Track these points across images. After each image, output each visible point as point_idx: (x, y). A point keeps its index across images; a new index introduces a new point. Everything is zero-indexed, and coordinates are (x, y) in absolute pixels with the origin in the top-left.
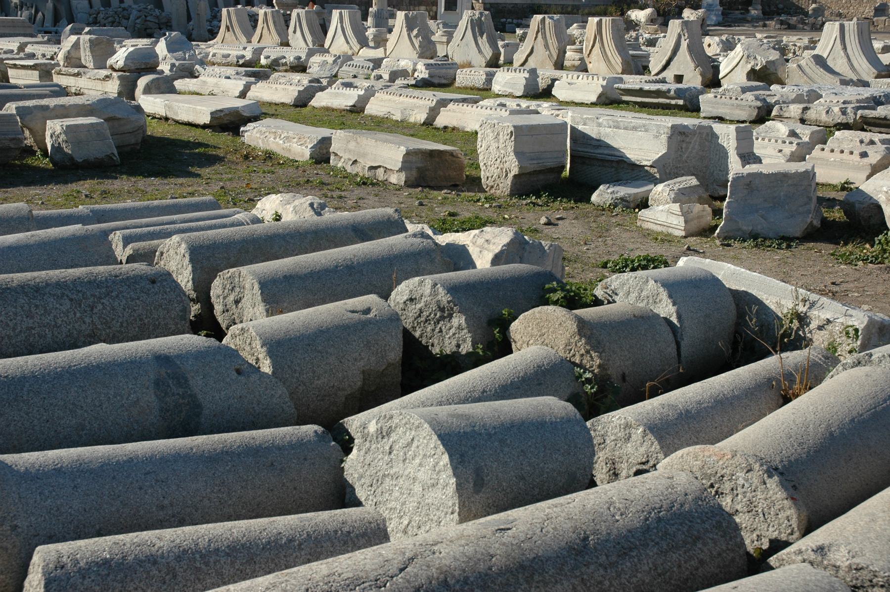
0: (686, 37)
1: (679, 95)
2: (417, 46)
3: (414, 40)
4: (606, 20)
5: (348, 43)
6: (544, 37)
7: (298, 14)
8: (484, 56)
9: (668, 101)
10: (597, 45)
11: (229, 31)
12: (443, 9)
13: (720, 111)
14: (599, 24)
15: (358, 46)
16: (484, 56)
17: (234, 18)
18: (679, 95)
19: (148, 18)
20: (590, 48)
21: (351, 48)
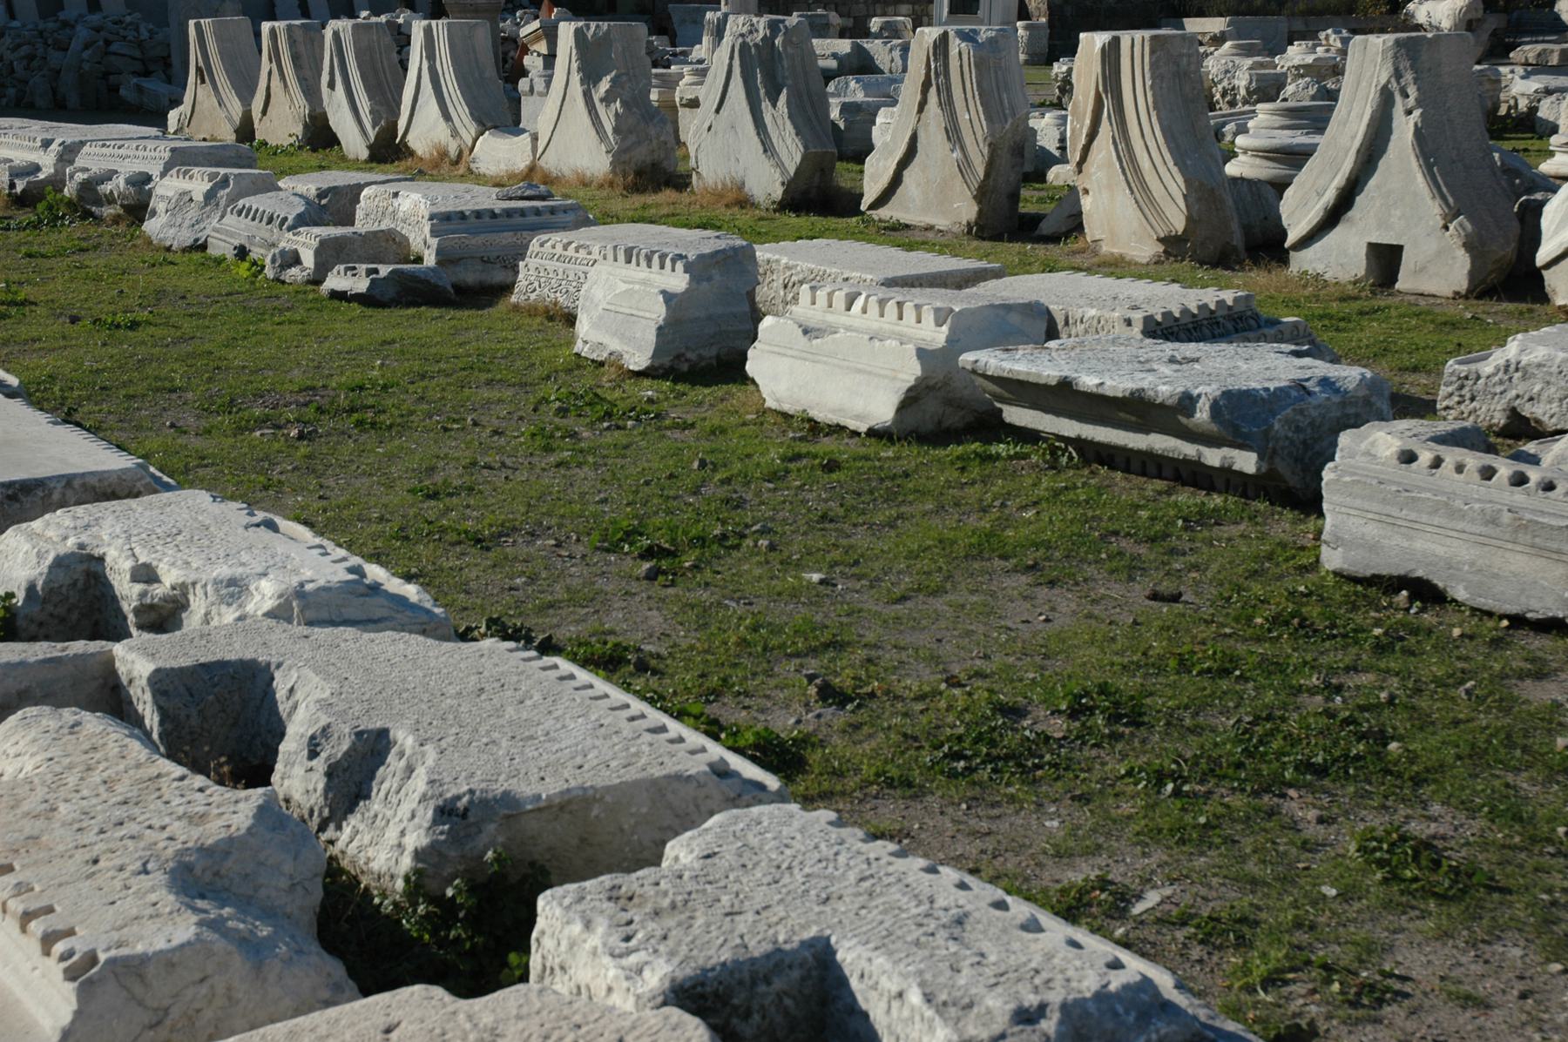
0: (1411, 101)
1: (1236, 430)
2: (609, 127)
3: (601, 108)
4: (1134, 41)
5: (447, 116)
6: (947, 104)
7: (336, 35)
8: (780, 165)
9: (1188, 450)
10: (1105, 130)
11: (203, 81)
12: (946, 10)
13: (1419, 545)
14: (1111, 55)
15: (473, 128)
16: (780, 165)
17: (212, 48)
18: (1236, 430)
19: (114, 47)
20: (1083, 141)
21: (455, 133)
